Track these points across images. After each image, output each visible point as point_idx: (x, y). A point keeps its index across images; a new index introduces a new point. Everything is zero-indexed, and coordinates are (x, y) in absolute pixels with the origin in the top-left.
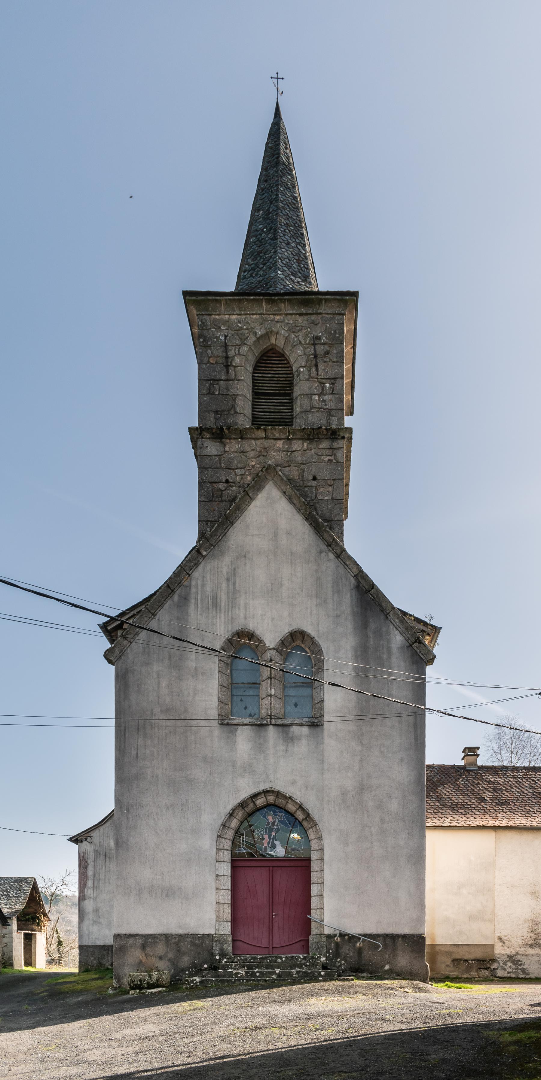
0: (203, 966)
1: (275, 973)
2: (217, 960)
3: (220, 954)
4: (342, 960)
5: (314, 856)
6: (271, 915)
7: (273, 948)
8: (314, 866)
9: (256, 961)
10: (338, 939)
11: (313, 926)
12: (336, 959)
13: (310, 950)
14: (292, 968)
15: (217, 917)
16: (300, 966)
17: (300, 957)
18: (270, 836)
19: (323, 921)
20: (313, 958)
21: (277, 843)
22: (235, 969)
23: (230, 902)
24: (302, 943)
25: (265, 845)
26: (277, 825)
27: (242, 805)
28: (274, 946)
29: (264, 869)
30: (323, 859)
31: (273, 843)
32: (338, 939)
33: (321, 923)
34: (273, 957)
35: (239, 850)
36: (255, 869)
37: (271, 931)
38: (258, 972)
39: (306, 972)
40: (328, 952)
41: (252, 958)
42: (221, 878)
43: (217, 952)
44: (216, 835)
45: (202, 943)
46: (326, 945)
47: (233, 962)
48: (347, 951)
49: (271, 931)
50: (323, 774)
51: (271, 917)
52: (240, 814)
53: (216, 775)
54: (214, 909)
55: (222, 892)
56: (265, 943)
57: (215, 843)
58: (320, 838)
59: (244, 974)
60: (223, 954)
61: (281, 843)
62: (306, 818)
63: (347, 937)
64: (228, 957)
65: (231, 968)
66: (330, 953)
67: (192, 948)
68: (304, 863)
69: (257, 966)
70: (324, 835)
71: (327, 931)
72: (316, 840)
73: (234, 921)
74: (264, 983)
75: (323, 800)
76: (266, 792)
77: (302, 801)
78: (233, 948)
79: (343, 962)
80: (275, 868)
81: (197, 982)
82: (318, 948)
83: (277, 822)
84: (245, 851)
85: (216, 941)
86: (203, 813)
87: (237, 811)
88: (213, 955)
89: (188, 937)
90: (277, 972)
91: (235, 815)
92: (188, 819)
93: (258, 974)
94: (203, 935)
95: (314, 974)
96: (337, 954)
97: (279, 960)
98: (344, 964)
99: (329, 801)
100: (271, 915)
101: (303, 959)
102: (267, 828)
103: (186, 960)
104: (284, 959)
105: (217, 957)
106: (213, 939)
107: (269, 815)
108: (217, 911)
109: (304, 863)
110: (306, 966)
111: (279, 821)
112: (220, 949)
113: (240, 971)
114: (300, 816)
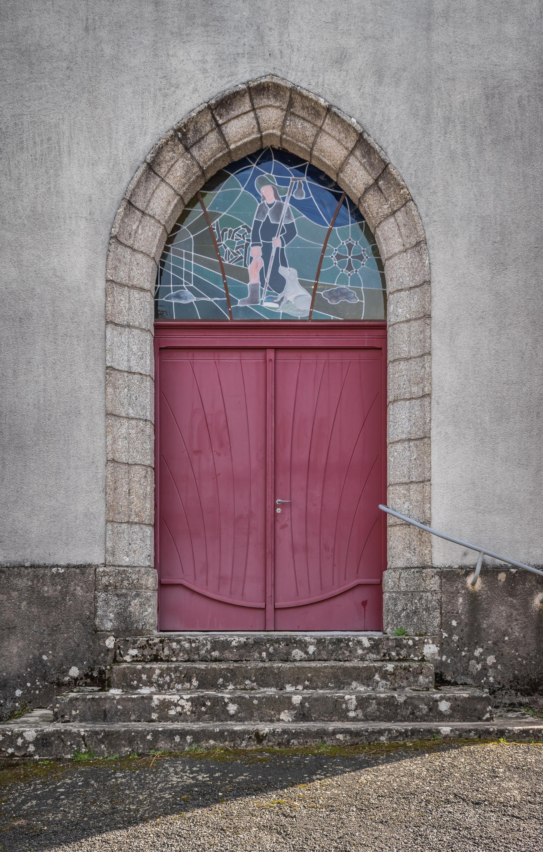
0: (65, 672)
1: (285, 703)
2: (27, 686)
3: (117, 633)
4: (488, 651)
5: (400, 308)
6: (270, 503)
7: (275, 609)
8: (400, 341)
9: (227, 654)
10: (474, 582)
11: (396, 540)
12: (471, 651)
13: (387, 618)
14: (340, 685)
15: (109, 507)
16: (365, 676)
17: (359, 643)
18: (266, 250)
19: (428, 522)
20: (399, 645)
21: (288, 273)
22: (160, 688)
23: (149, 460)
24: (360, 595)
25: (254, 279)
26: (289, 217)
27: (184, 136)
28: (279, 604)
29: (252, 360)
30: (430, 317)
31: (275, 274)
32: (474, 582)
33: (422, 529)
34: (278, 641)
35: (178, 296)
36: (224, 356)
37: (270, 555)
38: (232, 700)
39: (390, 703)
40: (444, 625)
41: (216, 645)
42: (121, 380)
43: (109, 625)
44: (105, 237)
45: (64, 593)
46: (440, 602)
47: (156, 659)
48: (502, 624)
49: (270, 555)
50: (429, 29)
51: (270, 510)
52: (178, 171)
53: (103, 34)
54: (101, 483)
55: (123, 428)
56: (252, 595)
57: (101, 261)
58: (420, 245)
59: (188, 706)
60: (127, 630)
61: (300, 274)
62: (376, 181)
63: (502, 577)
64: (142, 640)
65: (149, 683)
66: (451, 631)
67: (34, 610)
68: (364, 339)
69: (232, 676)
70: (433, 233)
71: (442, 556)
72: (408, 256)
73: (164, 524)
74: (254, 746)
75: (428, 118)
76: (258, 90)
77: (367, 120)
78: (161, 609)
79: (491, 660)
80: (281, 355)
81: (26, 743)
82: (415, 612)
83: (287, 204)
84: (194, 299)
85: (106, 588)
86: (65, 160)
87: (168, 155)
88: (96, 634)
89: (19, 575)
90: (296, 699)
91: (163, 170)
92: (19, 180)
93: (232, 708)
94: (68, 567)
95: (416, 707)
96: (473, 634)
97: (297, 653)
98: (494, 666)
99: (448, 120)
100: (270, 503)
101: (370, 650)
102: (257, 223)
103: (15, 650)
104: (311, 649)
105: (110, 643)
106: (96, 582)
107: (264, 182)
108: (110, 489)
109: (364, 339)
110: (385, 675)
111: (293, 201)
112: (118, 615)
113: (175, 698)
114: (356, 177)
